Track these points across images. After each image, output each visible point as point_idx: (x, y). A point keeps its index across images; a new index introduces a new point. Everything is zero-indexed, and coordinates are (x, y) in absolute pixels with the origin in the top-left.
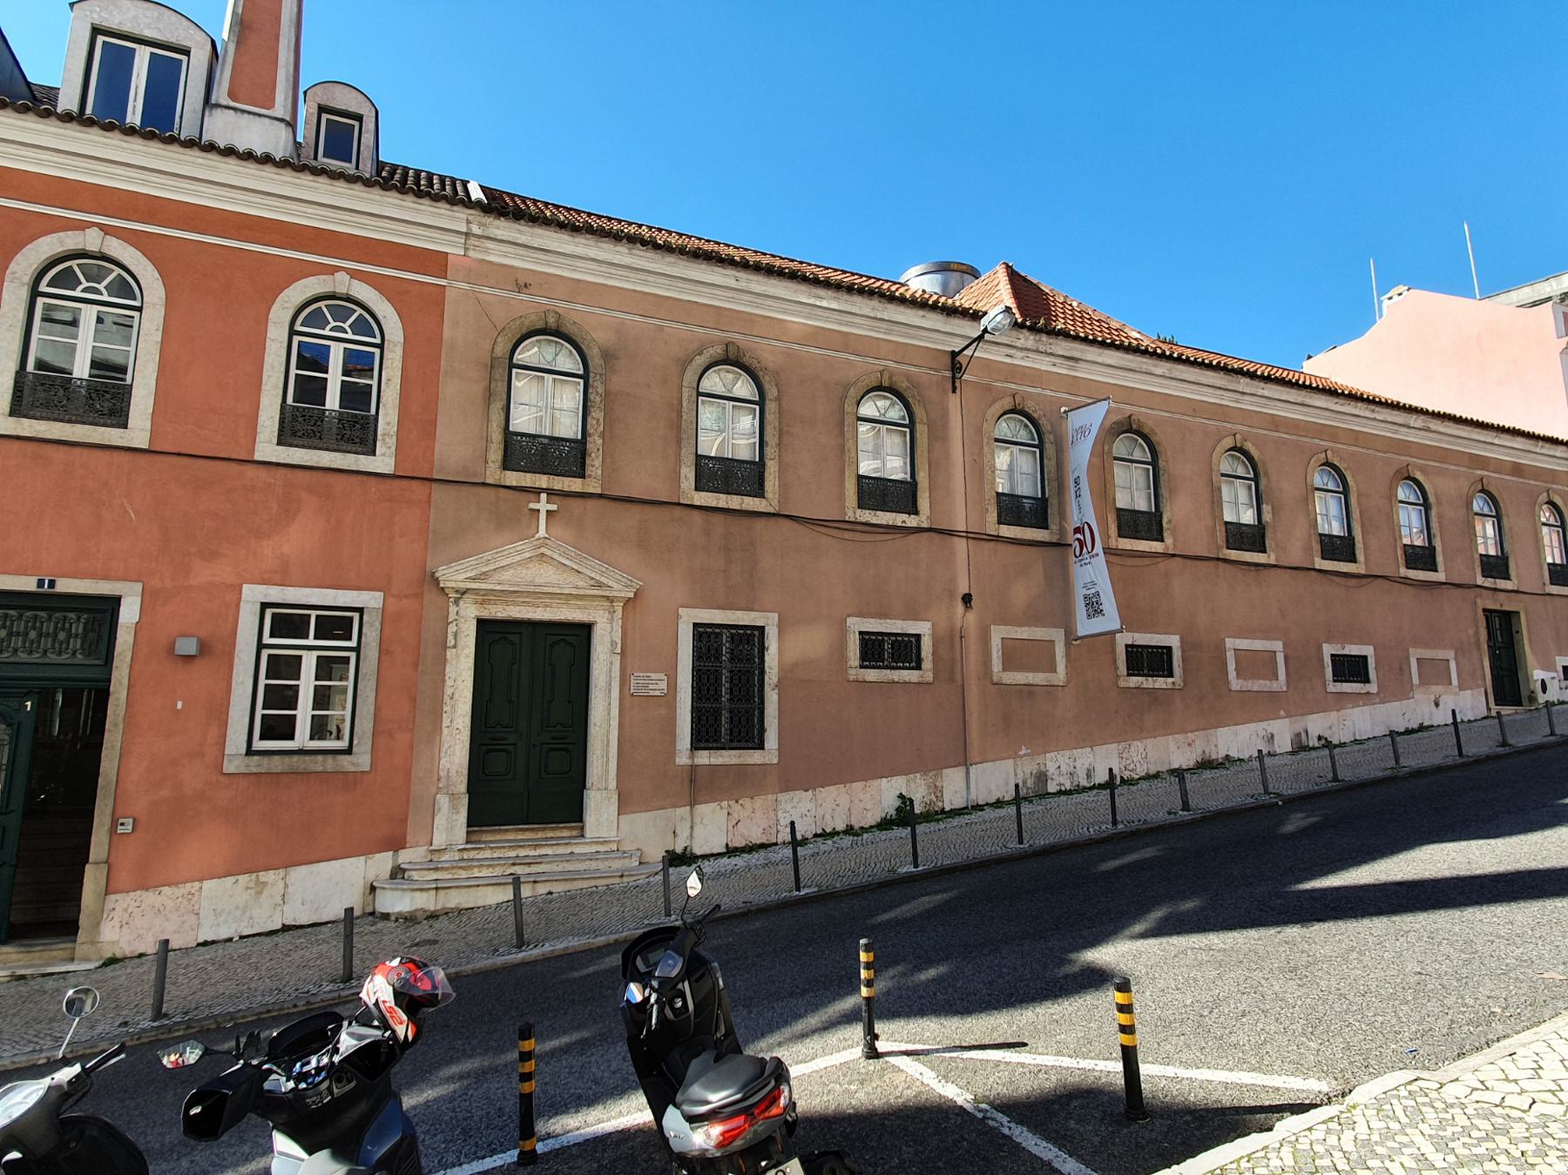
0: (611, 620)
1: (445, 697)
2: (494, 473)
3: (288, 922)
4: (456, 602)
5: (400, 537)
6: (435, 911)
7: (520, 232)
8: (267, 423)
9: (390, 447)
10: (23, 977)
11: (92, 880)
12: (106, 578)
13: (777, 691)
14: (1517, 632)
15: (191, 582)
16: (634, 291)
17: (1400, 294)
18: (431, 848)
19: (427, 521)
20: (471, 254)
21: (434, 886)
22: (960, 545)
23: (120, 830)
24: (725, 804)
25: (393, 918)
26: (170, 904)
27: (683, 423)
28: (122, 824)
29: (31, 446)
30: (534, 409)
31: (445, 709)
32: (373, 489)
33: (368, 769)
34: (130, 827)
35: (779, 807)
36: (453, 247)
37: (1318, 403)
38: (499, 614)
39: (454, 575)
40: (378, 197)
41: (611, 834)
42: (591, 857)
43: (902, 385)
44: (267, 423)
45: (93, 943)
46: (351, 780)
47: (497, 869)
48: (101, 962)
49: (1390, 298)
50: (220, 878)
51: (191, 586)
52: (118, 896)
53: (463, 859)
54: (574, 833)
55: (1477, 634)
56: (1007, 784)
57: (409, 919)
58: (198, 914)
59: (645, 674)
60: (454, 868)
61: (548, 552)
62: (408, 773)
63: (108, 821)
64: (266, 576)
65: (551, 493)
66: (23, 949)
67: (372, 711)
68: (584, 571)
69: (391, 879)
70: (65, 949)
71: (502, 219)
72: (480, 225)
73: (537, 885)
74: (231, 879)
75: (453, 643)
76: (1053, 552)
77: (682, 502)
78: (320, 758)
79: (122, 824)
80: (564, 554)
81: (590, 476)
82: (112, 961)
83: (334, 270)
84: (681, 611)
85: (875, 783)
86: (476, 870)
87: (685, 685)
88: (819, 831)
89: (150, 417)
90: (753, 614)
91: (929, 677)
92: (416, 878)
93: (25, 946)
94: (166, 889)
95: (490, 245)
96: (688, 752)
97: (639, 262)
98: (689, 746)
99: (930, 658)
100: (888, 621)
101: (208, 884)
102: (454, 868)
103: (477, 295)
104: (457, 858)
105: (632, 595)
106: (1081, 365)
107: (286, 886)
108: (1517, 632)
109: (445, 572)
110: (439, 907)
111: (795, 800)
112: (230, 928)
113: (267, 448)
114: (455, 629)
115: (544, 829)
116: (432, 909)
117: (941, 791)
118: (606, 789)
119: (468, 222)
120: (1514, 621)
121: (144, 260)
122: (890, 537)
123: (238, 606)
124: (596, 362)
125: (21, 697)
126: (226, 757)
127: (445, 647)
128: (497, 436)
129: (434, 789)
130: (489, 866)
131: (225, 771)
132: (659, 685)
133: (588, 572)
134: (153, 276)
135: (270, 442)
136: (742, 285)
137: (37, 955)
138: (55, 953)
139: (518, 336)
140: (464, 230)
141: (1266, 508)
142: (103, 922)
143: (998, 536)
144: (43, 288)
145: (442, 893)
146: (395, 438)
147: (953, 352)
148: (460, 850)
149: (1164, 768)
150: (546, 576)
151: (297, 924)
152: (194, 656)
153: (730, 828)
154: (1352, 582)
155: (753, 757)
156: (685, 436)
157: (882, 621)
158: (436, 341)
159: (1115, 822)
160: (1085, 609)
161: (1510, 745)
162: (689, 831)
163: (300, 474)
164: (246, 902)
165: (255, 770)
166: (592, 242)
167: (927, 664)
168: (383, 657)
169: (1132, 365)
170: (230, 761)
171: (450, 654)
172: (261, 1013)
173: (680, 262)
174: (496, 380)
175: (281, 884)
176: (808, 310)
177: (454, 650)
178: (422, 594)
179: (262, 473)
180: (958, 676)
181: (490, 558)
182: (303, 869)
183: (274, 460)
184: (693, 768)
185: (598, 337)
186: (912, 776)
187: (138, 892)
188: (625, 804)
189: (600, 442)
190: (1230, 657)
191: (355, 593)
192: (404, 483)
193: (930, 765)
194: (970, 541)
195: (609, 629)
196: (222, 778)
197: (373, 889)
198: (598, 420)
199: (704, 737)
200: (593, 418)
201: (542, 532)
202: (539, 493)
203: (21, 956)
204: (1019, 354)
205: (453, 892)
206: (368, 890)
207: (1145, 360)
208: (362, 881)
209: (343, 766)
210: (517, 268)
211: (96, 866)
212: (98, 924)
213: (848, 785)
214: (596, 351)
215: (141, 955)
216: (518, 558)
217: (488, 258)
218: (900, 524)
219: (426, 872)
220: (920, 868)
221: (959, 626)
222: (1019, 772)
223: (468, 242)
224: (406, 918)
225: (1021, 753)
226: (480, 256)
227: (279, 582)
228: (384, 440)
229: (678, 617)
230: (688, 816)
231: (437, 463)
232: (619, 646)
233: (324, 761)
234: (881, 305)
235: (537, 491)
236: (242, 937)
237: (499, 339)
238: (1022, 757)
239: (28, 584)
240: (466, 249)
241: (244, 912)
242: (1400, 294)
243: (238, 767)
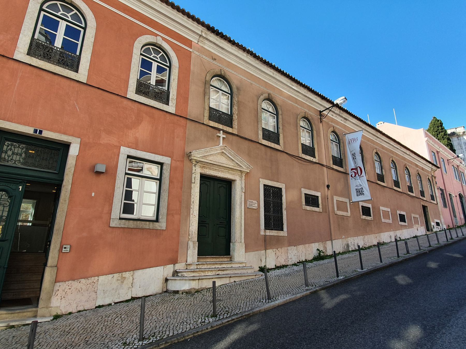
0: (241, 180)
1: (191, 202)
2: (206, 121)
3: (134, 296)
4: (195, 165)
5: (177, 138)
6: (198, 289)
7: (217, 40)
8: (132, 84)
9: (174, 104)
10: (13, 327)
11: (49, 275)
12: (65, 133)
13: (286, 211)
14: (427, 212)
15: (101, 142)
16: (244, 70)
17: (381, 124)
18: (187, 263)
19: (185, 134)
20: (199, 43)
21: (198, 278)
22: (325, 169)
23: (64, 250)
24: (274, 250)
25: (180, 293)
26: (84, 287)
27: (259, 116)
28: (65, 248)
29: (36, 70)
30: (215, 101)
31: (191, 207)
32: (168, 118)
33: (165, 229)
34: (68, 249)
35: (288, 252)
36: (193, 39)
37: (392, 144)
38: (207, 173)
39: (197, 155)
40: (175, 13)
41: (243, 260)
42: (239, 268)
43: (310, 118)
44: (132, 84)
45: (47, 307)
46: (158, 232)
47: (213, 272)
48: (52, 318)
49: (379, 124)
50: (106, 275)
51: (100, 144)
52: (61, 284)
53: (198, 269)
54: (229, 260)
55: (422, 211)
56: (341, 247)
57: (188, 293)
58: (96, 292)
59: (251, 201)
60: (200, 271)
61: (225, 152)
62: (179, 231)
63: (58, 246)
64: (130, 145)
65: (225, 132)
66: (10, 312)
67: (167, 205)
68: (235, 160)
69: (173, 276)
70: (31, 311)
71: (213, 34)
72: (205, 33)
73: (231, 278)
74: (111, 276)
75: (194, 181)
76: (344, 175)
77: (259, 142)
78: (148, 223)
79: (65, 248)
80: (229, 153)
81: (234, 128)
82: (57, 317)
83: (156, 35)
84: (260, 179)
85: (311, 245)
86: (207, 272)
87: (262, 206)
88: (299, 261)
89: (88, 71)
90: (279, 183)
91: (321, 211)
92: (186, 275)
93: (9, 310)
94: (83, 281)
95: (206, 42)
96: (264, 230)
97: (248, 60)
98: (264, 228)
99: (321, 204)
100: (311, 191)
101: (101, 278)
102: (200, 271)
103: (201, 58)
104: (196, 268)
105: (249, 171)
106: (347, 122)
107: (133, 279)
108: (427, 212)
109: (194, 153)
110: (199, 288)
111: (292, 250)
112: (110, 299)
113: (132, 94)
114: (195, 176)
115: (219, 258)
116: (197, 288)
117: (326, 249)
118: (241, 242)
119: (202, 32)
120: (426, 209)
121: (89, 9)
122: (310, 164)
123: (118, 155)
124: (235, 90)
125: (18, 184)
126: (111, 219)
127: (191, 182)
128: (207, 108)
129: (187, 239)
130: (211, 271)
131: (111, 226)
132: (255, 206)
133: (236, 161)
134: (92, 16)
135: (133, 92)
136: (274, 76)
137: (17, 315)
138: (25, 314)
139: (213, 75)
140: (200, 34)
141: (383, 170)
142: (53, 297)
143: (333, 168)
144: (44, 7)
145: (200, 281)
146: (175, 101)
147: (320, 111)
148: (197, 265)
149: (372, 245)
150: (223, 161)
151: (137, 296)
152: (103, 173)
153: (276, 259)
154: (400, 194)
155: (281, 233)
156: (259, 121)
157: (309, 191)
158: (188, 70)
159: (398, 256)
160: (356, 193)
161: (453, 239)
162: (265, 260)
163: (143, 107)
164: (117, 287)
165: (123, 226)
166: (237, 50)
167: (320, 206)
168: (170, 184)
169: (358, 124)
170: (113, 221)
171: (193, 185)
172: (195, 333)
173: (260, 63)
174: (207, 88)
175: (131, 278)
176: (288, 89)
177: (194, 184)
178: (184, 161)
179: (130, 103)
180: (327, 211)
181: (208, 150)
182: (140, 271)
183: (134, 99)
184: (265, 236)
185: (235, 83)
186: (319, 243)
187: (70, 282)
188: (248, 249)
189: (237, 117)
190: (381, 211)
191: (161, 157)
192: (178, 118)
193: (322, 240)
194: (327, 169)
195: (240, 183)
196: (109, 229)
197: (167, 280)
198: (236, 110)
199: (267, 227)
200: (235, 108)
201: (221, 144)
202: (220, 131)
203: (7, 316)
204: (335, 115)
205: (204, 281)
206: (164, 282)
207: (361, 123)
208: (162, 277)
209: (156, 227)
210: (212, 53)
211: (51, 268)
212: (50, 297)
213: (305, 245)
214: (235, 86)
215: (70, 313)
216: (216, 152)
217: (204, 46)
218: (312, 160)
219: (190, 273)
220: (364, 270)
221: (326, 195)
222: (343, 243)
223: (200, 39)
224: (187, 293)
225: (343, 237)
226: (202, 45)
227: (135, 148)
228: (172, 101)
229: (259, 181)
230: (264, 254)
231: (188, 113)
232: (244, 189)
233: (149, 224)
234: (307, 92)
235: (219, 130)
236: (115, 303)
237: (208, 75)
238: (343, 238)
239: (29, 130)
240: (198, 41)
241: (116, 291)
242: (381, 124)
243: (116, 224)
